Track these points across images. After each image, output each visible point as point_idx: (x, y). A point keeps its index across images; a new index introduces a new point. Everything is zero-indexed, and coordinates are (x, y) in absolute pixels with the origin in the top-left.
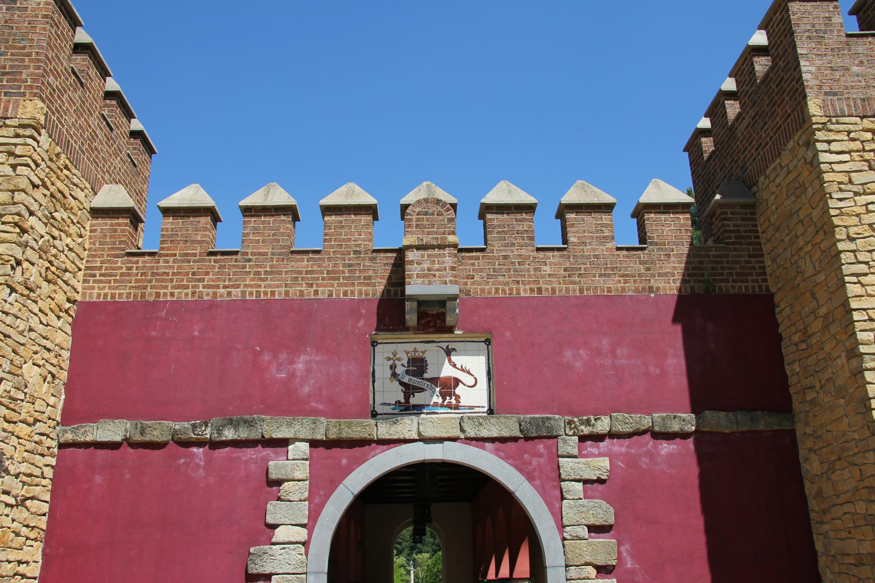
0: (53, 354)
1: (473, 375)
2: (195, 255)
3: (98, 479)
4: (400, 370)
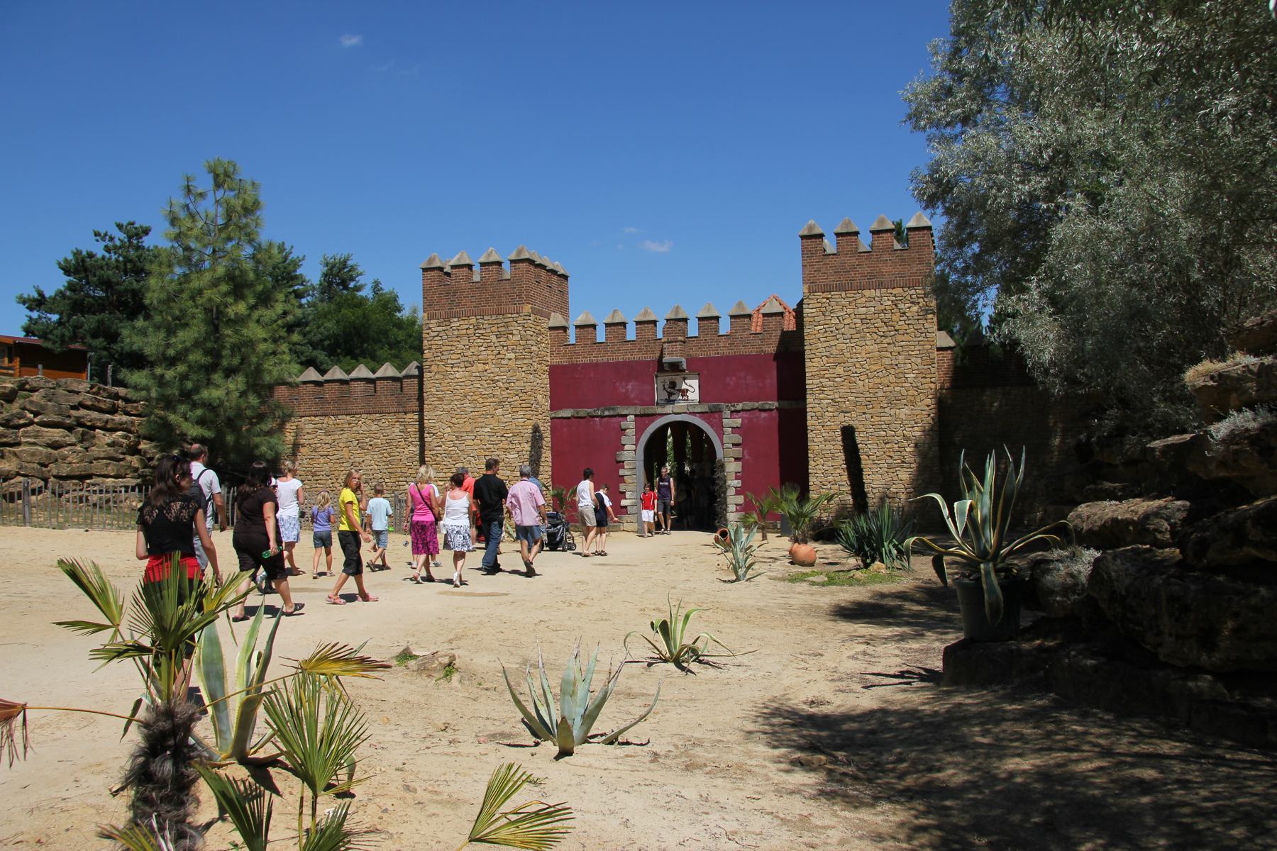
1: (441, 581)
3: (565, 430)
4: (666, 386)
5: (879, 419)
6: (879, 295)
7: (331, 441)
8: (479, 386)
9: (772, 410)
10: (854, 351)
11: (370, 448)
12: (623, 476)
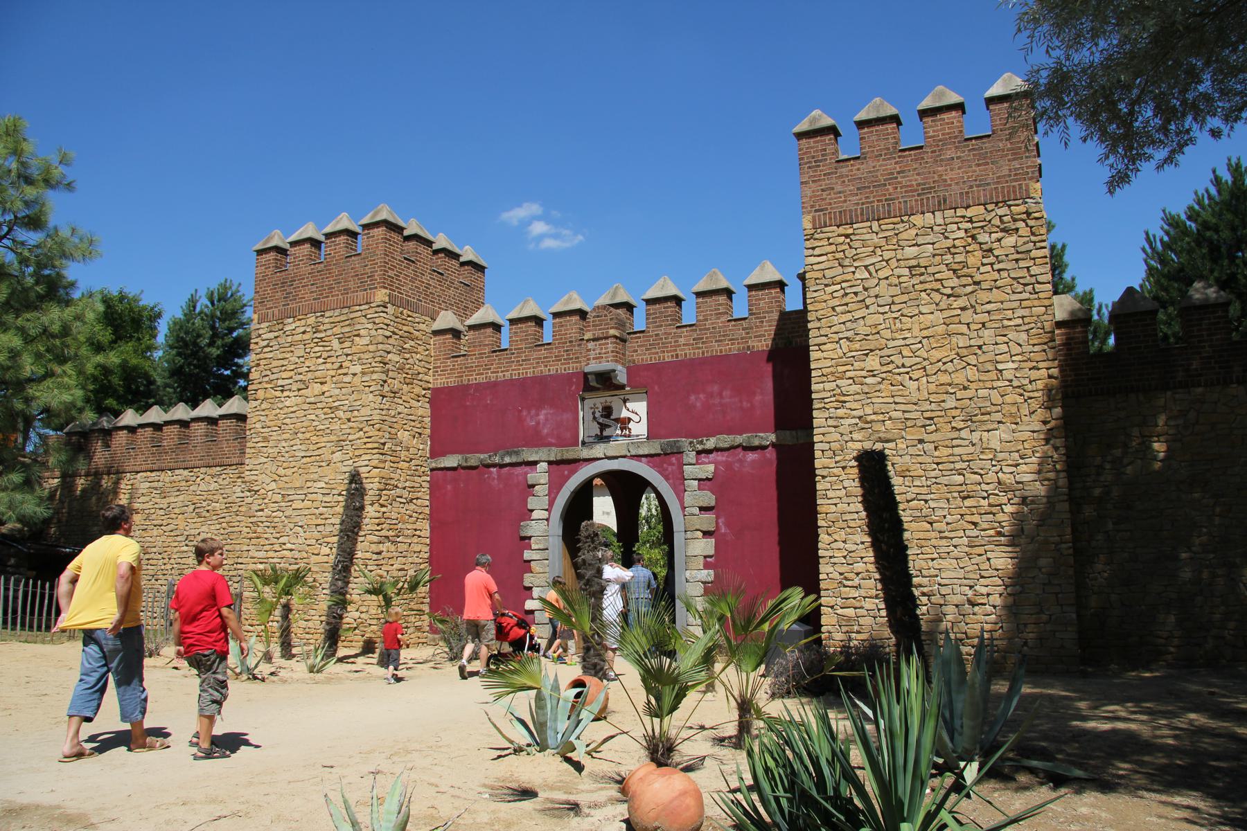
0: (417, 422)
2: (485, 353)
3: (449, 487)
4: (598, 415)
5: (950, 451)
6: (940, 221)
7: (165, 506)
8: (313, 417)
9: (763, 448)
10: (898, 325)
11: (208, 515)
12: (529, 561)
